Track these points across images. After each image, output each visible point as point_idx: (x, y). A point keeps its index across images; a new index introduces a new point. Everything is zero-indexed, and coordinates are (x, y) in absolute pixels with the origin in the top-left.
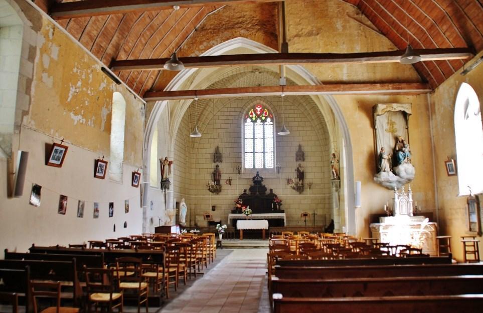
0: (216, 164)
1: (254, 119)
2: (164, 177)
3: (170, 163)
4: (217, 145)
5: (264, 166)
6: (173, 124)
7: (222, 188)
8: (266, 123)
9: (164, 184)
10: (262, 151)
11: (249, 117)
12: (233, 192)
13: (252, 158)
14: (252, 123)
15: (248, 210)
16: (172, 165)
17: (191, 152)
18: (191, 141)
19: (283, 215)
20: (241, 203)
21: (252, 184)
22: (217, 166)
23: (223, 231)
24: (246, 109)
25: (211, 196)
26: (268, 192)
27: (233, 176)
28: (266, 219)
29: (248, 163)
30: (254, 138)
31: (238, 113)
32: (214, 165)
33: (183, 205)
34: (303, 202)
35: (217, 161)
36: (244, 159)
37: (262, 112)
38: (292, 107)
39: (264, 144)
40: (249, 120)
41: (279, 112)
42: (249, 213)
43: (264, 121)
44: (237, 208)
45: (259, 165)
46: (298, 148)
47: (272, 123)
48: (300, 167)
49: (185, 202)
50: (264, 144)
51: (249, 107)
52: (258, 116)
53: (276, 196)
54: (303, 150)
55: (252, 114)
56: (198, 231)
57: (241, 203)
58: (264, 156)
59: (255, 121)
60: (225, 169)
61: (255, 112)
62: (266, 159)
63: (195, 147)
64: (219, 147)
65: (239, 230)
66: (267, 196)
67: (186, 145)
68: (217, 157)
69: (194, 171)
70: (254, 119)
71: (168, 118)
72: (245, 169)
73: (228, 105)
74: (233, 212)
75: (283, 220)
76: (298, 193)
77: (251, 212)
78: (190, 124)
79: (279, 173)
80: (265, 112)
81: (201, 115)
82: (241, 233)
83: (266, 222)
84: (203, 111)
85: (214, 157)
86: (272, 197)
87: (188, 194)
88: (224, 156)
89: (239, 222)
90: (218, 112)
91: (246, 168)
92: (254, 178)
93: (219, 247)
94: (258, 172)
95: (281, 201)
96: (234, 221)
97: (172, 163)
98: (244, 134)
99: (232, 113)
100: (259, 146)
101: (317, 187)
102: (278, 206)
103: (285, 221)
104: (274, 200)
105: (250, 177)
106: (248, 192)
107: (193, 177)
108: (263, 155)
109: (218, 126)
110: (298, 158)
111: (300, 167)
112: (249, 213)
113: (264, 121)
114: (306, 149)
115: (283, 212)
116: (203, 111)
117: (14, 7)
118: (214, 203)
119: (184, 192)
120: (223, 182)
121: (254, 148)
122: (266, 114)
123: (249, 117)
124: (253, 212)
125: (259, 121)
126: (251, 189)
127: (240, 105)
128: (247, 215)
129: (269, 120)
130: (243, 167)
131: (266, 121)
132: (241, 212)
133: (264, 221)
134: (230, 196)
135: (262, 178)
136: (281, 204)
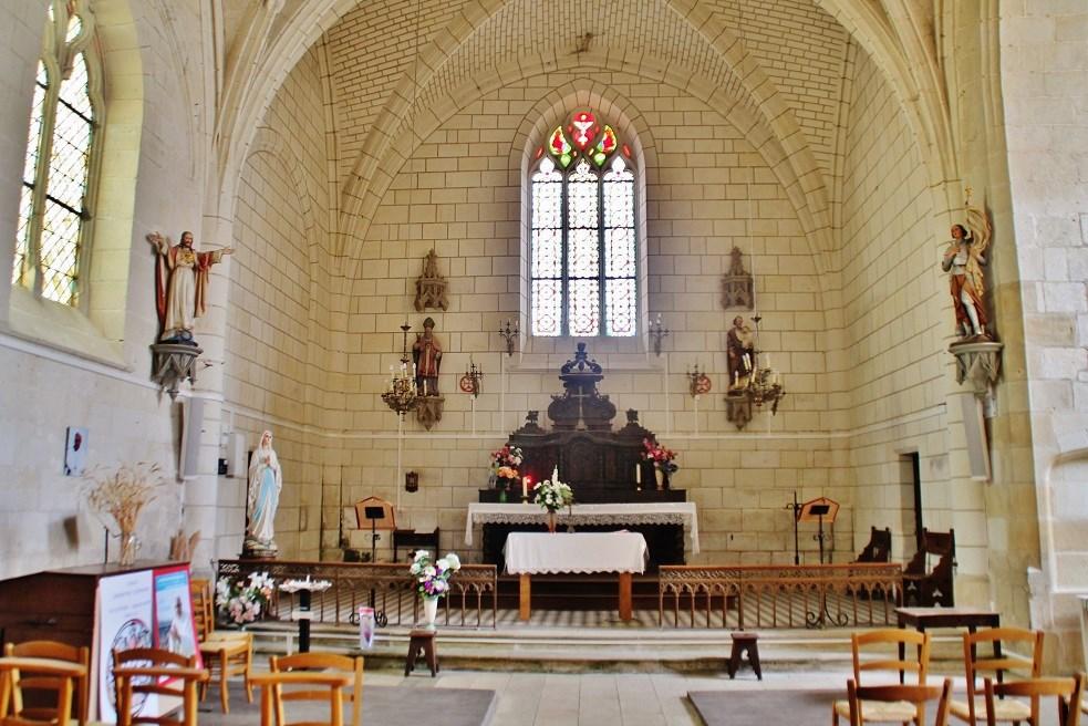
0: (425, 317)
1: (566, 160)
2: (171, 323)
3: (203, 264)
4: (428, 247)
5: (602, 326)
6: (235, 88)
7: (446, 406)
8: (607, 177)
9: (167, 355)
10: (596, 274)
11: (546, 152)
12: (496, 410)
13: (559, 297)
14: (558, 176)
15: (557, 486)
16: (220, 273)
17: (335, 272)
18: (333, 230)
19: (683, 511)
20: (518, 461)
21: (560, 390)
22: (429, 323)
23: (441, 585)
24: (540, 123)
25: (401, 427)
26: (619, 422)
27: (488, 362)
28: (633, 528)
29: (543, 317)
30: (565, 227)
31: (509, 135)
32: (416, 321)
33: (266, 460)
34: (751, 460)
35: (429, 304)
36: (529, 301)
37: (594, 136)
38: (709, 118)
39: (601, 248)
40: (547, 165)
41: (658, 133)
42: (559, 501)
43: (600, 170)
44: (503, 480)
45: (583, 324)
46: (727, 260)
47: (629, 176)
48: (740, 329)
49: (274, 447)
50: (601, 248)
51: (549, 114)
52: (580, 153)
53: (651, 437)
54: (746, 269)
55: (558, 144)
56: (323, 585)
57: (518, 461)
58: (602, 293)
59: (571, 168)
60: (460, 332)
61: (571, 134)
62: (608, 301)
63: (348, 251)
64: (436, 253)
65: (518, 575)
66: (614, 436)
67: (312, 239)
68: (429, 291)
69: (340, 341)
70: (566, 160)
71: (210, 71)
72: (530, 337)
73: (475, 108)
74: (487, 496)
75: (1059, 580)
76: (732, 426)
77: (569, 494)
78: (332, 164)
79: (658, 351)
80: (605, 138)
81: (371, 134)
82: (525, 587)
83: (638, 543)
84: (381, 117)
85: (419, 289)
86: (638, 438)
87: (312, 425)
88: (454, 286)
89: (514, 539)
90: (438, 128)
91: (536, 333)
92: (565, 369)
93: (420, 660)
94: (581, 346)
95: (671, 455)
96: (494, 537)
97: (211, 262)
98: (530, 212)
99: (486, 136)
100: (583, 263)
101: (799, 406)
102: (659, 475)
103: (694, 534)
104: (647, 452)
105: (551, 366)
106: (545, 423)
107: (338, 363)
108: (596, 288)
109: (438, 181)
110: (733, 296)
111: (740, 329)
112: (559, 501)
113: (600, 170)
114: (755, 265)
115: (679, 496)
116: (381, 117)
117: (631, 672)
118: (415, 462)
119: (287, 415)
120: (448, 384)
121: (564, 261)
122: (608, 143)
123: (546, 152)
124: (579, 498)
125: (583, 167)
126: (557, 408)
127: (517, 108)
128: (552, 508)
129: (619, 163)
130: (523, 329)
131: (609, 168)
132: (515, 496)
133: (623, 534)
134: (474, 436)
135: (597, 369)
136: (674, 468)
